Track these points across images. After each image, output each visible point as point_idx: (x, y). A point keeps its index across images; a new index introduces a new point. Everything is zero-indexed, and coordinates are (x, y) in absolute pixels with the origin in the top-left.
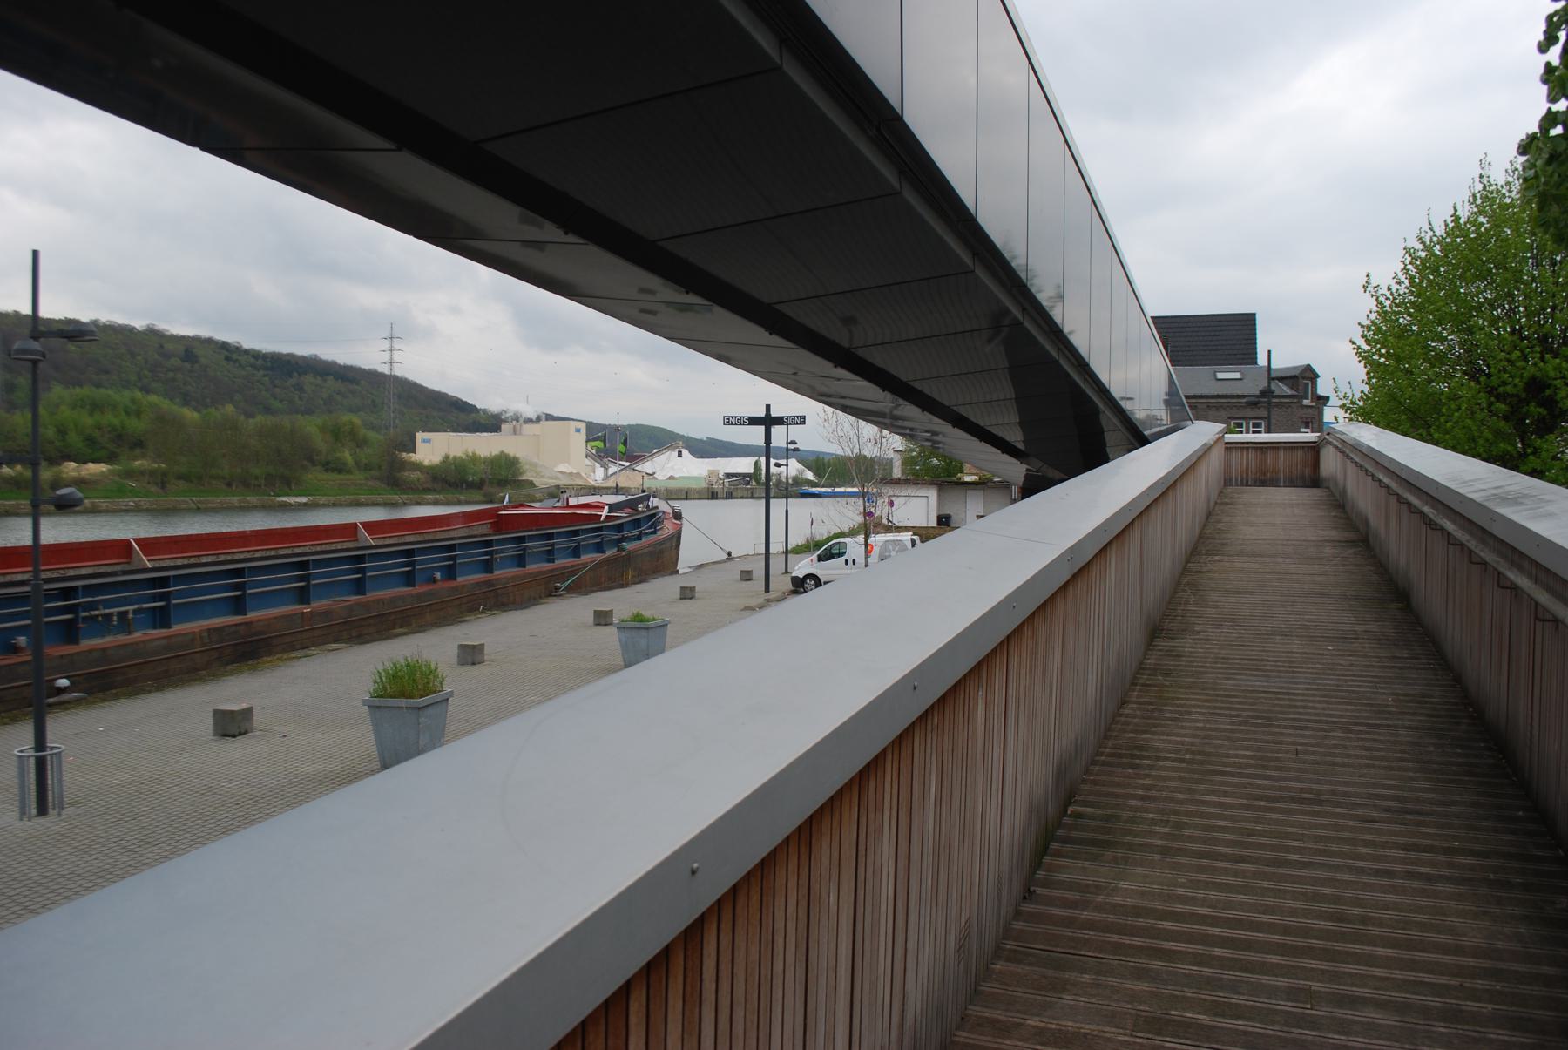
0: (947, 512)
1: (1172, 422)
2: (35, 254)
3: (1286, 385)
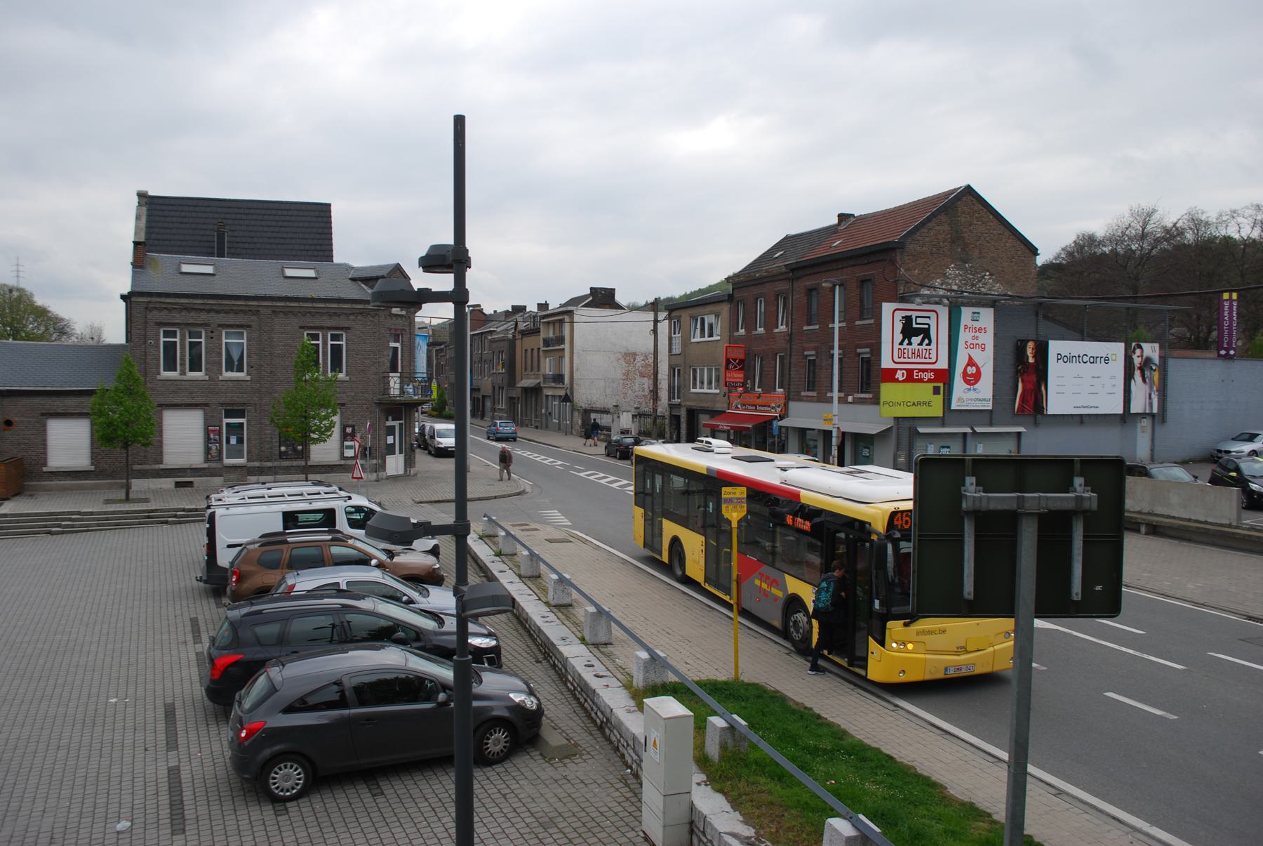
2: (459, 122)
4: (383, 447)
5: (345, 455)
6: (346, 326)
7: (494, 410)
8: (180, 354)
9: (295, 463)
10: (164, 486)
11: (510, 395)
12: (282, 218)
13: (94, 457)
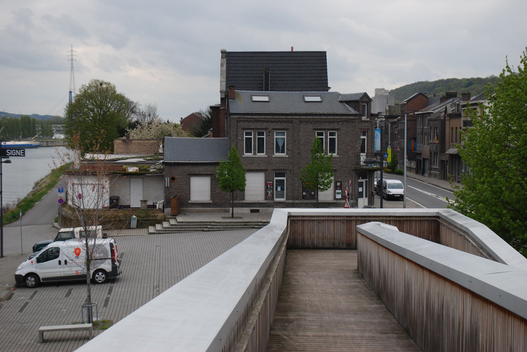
0: (116, 194)
3: (351, 106)
4: (357, 193)
5: (337, 197)
6: (337, 128)
7: (431, 169)
8: (254, 144)
9: (310, 201)
10: (245, 212)
11: (441, 159)
12: (299, 62)
13: (212, 196)
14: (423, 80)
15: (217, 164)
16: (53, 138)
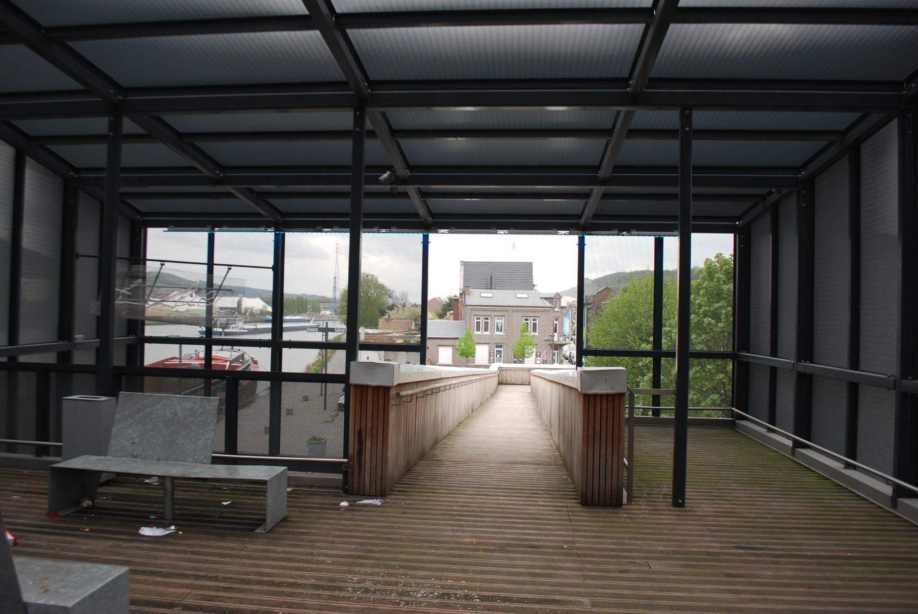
1: (384, 180)
3: (548, 301)
8: (482, 326)
14: (622, 271)
15: (457, 339)
16: (321, 314)
